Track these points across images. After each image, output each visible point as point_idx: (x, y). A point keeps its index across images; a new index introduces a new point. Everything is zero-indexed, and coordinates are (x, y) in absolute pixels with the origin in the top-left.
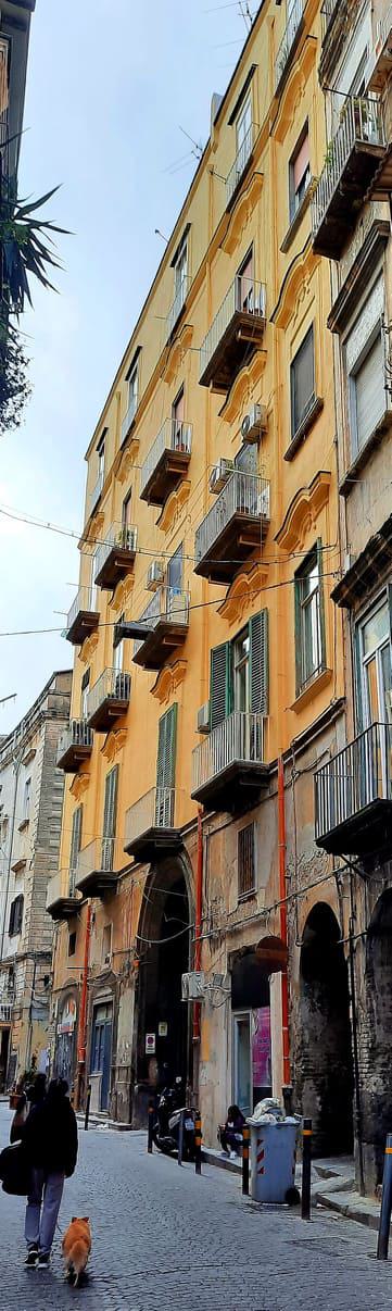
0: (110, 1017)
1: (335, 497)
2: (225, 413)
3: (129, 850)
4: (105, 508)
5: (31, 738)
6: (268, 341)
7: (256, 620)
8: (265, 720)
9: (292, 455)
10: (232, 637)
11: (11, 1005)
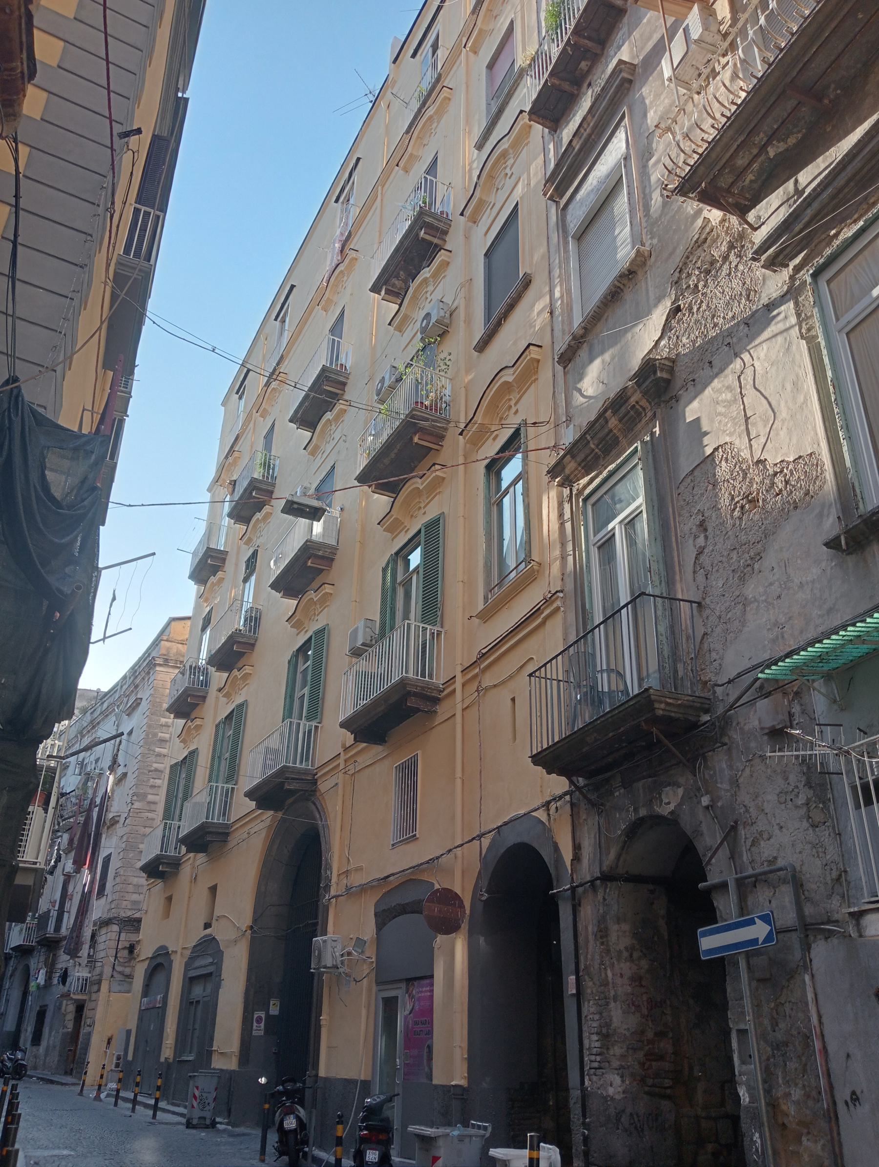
0: (209, 990)
1: (546, 373)
2: (310, 448)
3: (250, 794)
4: (244, 446)
5: (136, 687)
6: (454, 241)
7: (320, 633)
8: (317, 727)
9: (483, 345)
10: (297, 647)
11: (89, 975)
